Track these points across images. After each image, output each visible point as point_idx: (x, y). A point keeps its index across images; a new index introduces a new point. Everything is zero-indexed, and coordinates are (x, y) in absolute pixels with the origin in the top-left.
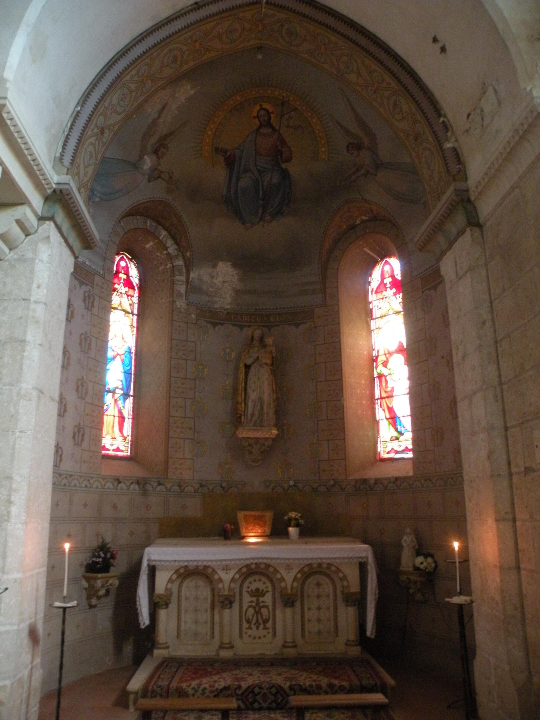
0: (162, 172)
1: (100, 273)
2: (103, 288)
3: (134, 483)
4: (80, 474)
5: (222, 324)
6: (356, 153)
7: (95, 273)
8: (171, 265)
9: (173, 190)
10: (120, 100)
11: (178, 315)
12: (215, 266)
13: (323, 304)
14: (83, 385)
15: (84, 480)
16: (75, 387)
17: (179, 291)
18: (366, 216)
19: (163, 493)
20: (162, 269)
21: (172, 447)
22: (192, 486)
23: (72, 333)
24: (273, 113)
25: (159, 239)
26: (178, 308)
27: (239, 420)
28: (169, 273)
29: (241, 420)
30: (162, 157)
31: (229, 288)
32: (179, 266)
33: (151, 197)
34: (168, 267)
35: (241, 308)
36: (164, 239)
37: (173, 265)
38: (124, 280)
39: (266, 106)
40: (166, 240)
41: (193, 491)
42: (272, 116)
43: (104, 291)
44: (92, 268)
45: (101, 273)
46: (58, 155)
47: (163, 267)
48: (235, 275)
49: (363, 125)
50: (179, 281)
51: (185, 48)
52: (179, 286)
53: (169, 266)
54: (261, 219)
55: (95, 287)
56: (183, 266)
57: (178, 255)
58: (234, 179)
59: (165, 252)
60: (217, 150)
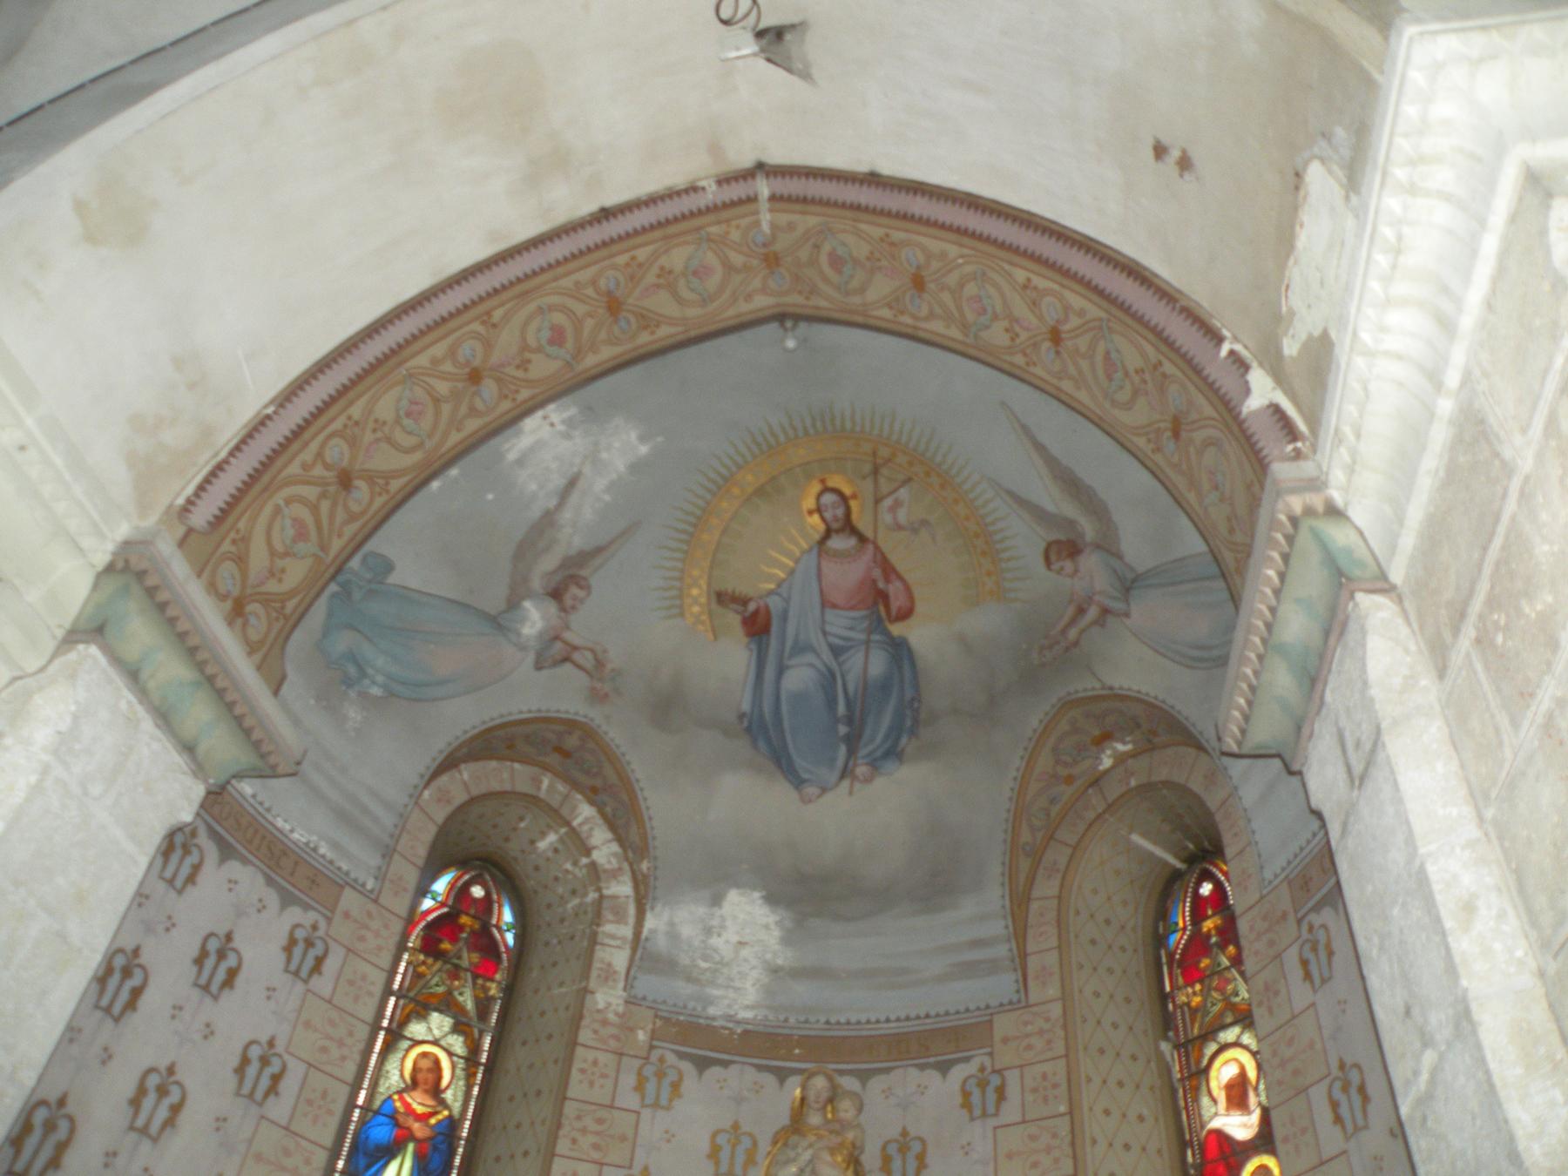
0: (575, 648)
1: (363, 885)
2: (367, 928)
5: (725, 1064)
6: (1068, 565)
7: (347, 884)
10: (402, 413)
12: (717, 900)
13: (1019, 1001)
14: (50, 1127)
17: (609, 965)
18: (1124, 743)
23: (212, 1033)
24: (854, 496)
26: (599, 1011)
30: (573, 608)
33: (543, 708)
35: (786, 1020)
36: (585, 828)
39: (836, 481)
42: (853, 504)
46: (180, 501)
48: (773, 927)
49: (1072, 484)
50: (613, 937)
51: (580, 309)
52: (613, 950)
53: (592, 896)
54: (844, 774)
55: (338, 918)
57: (620, 869)
58: (770, 673)
59: (584, 861)
60: (723, 598)
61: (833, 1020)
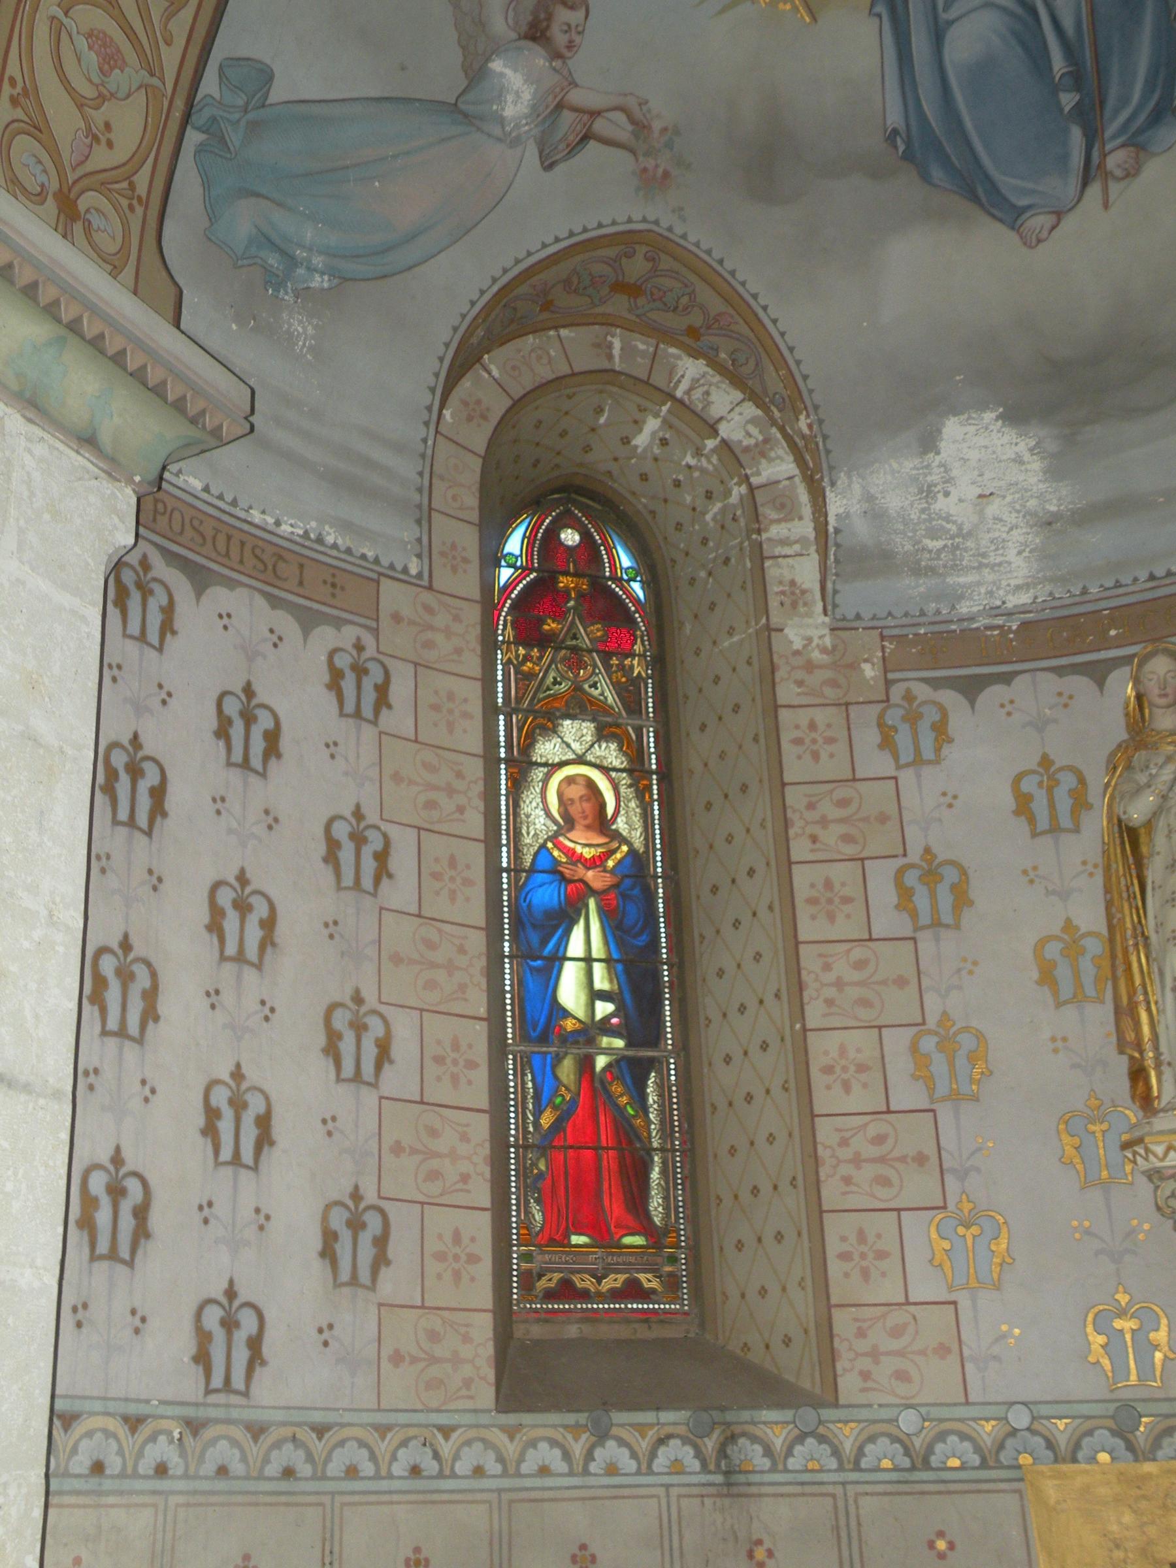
0: (595, 114)
1: (405, 570)
2: (431, 628)
3: (670, 1436)
4: (380, 1418)
5: (1006, 679)
7: (380, 574)
8: (743, 489)
9: (666, 175)
11: (800, 683)
12: (929, 443)
15: (404, 1443)
16: (321, 1040)
17: (793, 583)
19: (824, 1477)
20: (714, 519)
21: (845, 1256)
22: (963, 1437)
25: (672, 397)
26: (797, 653)
27: (581, 1039)
28: (742, 522)
29: (1149, 1088)
31: (1012, 518)
32: (778, 482)
34: (734, 499)
36: (697, 394)
37: (750, 486)
38: (581, 596)
40: (707, 393)
41: (976, 1460)
43: (439, 638)
44: (363, 557)
45: (414, 571)
47: (719, 505)
48: (1027, 457)
50: (785, 542)
53: (738, 491)
56: (797, 480)
57: (766, 441)
59: (710, 444)
61: (1160, 572)
